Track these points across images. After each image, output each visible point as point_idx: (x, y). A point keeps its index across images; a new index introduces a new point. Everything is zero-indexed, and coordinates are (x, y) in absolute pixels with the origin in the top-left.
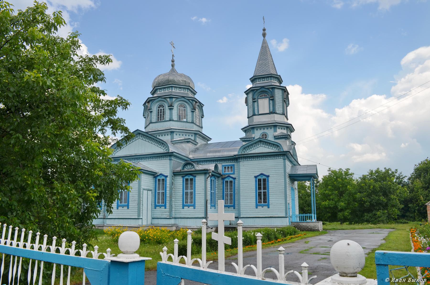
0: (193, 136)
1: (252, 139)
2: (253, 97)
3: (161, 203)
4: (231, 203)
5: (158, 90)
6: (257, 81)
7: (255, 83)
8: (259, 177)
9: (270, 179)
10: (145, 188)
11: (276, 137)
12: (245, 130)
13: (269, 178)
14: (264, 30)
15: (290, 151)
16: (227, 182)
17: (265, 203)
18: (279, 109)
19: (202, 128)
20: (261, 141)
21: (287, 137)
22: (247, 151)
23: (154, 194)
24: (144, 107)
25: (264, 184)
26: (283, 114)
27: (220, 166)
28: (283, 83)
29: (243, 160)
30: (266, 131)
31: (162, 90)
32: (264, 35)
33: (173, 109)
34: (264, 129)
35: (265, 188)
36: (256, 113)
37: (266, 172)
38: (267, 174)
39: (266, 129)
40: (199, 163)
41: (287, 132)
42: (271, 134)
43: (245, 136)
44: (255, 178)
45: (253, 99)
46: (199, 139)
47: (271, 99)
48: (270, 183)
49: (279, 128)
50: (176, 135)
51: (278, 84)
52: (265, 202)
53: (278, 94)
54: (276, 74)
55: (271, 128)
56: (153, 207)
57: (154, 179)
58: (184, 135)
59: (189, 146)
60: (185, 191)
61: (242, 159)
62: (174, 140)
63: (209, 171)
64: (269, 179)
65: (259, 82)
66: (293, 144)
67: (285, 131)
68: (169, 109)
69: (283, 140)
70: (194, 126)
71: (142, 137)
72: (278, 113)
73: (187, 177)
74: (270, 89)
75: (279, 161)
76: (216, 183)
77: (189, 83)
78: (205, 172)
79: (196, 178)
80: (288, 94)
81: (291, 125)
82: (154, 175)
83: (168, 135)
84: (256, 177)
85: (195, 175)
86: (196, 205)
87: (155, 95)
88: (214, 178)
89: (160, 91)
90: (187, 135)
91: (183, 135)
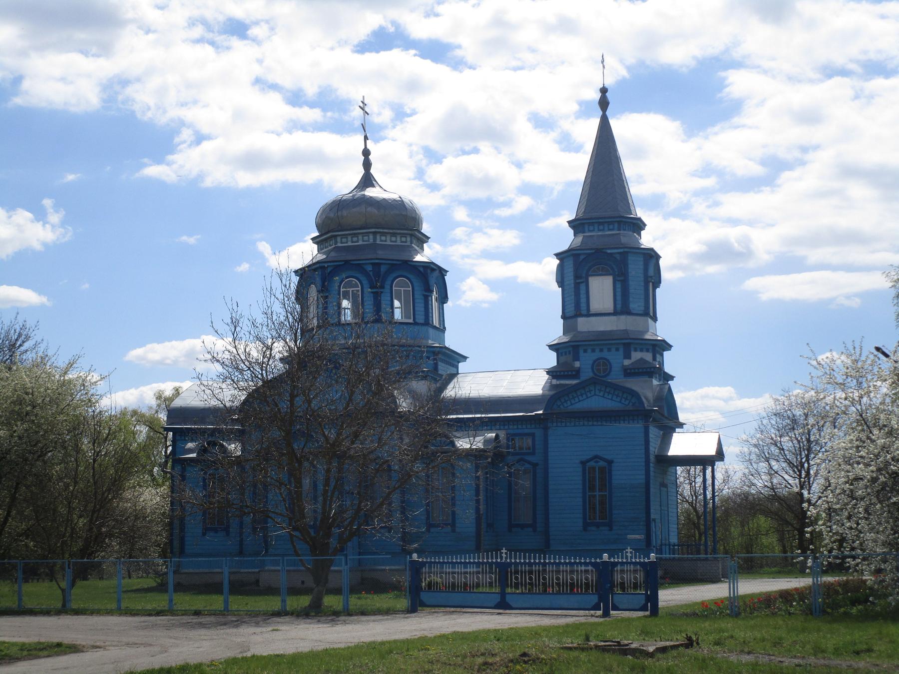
8: (592, 464)
11: (629, 371)
13: (613, 464)
31: (349, 238)
33: (382, 292)
36: (584, 311)
49: (636, 350)
55: (617, 350)
60: (588, 494)
68: (372, 292)
75: (637, 426)
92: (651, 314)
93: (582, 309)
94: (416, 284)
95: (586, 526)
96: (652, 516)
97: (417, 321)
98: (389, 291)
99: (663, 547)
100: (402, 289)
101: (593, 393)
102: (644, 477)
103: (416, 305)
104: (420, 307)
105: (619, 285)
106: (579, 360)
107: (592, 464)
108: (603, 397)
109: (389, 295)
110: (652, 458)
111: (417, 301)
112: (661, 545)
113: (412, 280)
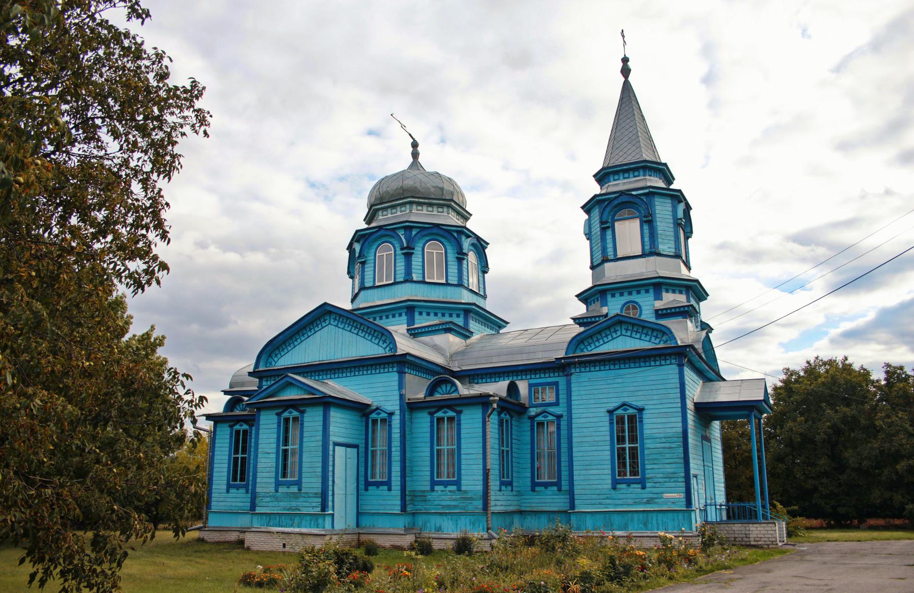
0: (462, 316)
1: (597, 319)
2: (601, 218)
3: (448, 477)
4: (382, 476)
5: (380, 213)
6: (612, 178)
7: (607, 185)
8: (620, 412)
9: (646, 415)
10: (340, 440)
11: (660, 312)
12: (584, 297)
13: (644, 412)
14: (625, 60)
15: (696, 346)
16: (375, 422)
17: (635, 475)
18: (665, 247)
19: (484, 297)
20: (621, 323)
21: (689, 312)
22: (589, 348)
23: (362, 455)
24: (350, 252)
25: (632, 427)
26: (677, 256)
27: (523, 387)
28: (675, 182)
29: (578, 370)
30: (635, 297)
32: (626, 71)
33: (413, 253)
34: (630, 293)
35: (633, 439)
37: (634, 398)
38: (640, 404)
39: (634, 293)
40: (474, 379)
41: (688, 300)
42: (648, 306)
43: (585, 311)
44: (608, 414)
45: (602, 223)
46: (477, 324)
47: (645, 222)
48: (645, 427)
49: (667, 291)
50: (421, 313)
51: (663, 185)
52: (634, 473)
53: (663, 210)
54: (654, 159)
55: (647, 291)
56: (362, 487)
57: (364, 419)
58: (440, 315)
59: (452, 341)
61: (575, 368)
62: (416, 326)
63: (492, 398)
64: (644, 416)
65: (626, 181)
66: (706, 327)
67: (680, 299)
68: (403, 254)
69: (680, 319)
70: (465, 293)
71: (335, 319)
72: (665, 253)
73: (440, 414)
74: (642, 197)
75: (668, 371)
76: (514, 428)
77: (452, 194)
78: (483, 401)
79: (463, 417)
80: (688, 208)
81: (697, 281)
82: (361, 410)
83: (400, 315)
84: (610, 412)
85: (458, 409)
86: (463, 482)
87: (373, 225)
88: (508, 417)
89: (385, 213)
90: (447, 315)
91: (436, 314)
92: (684, 258)
93: (609, 254)
94: (449, 247)
95: (615, 484)
96: (692, 472)
97: (449, 282)
98: (421, 253)
99: (709, 507)
100: (435, 251)
101: (619, 333)
102: (680, 425)
103: (449, 267)
104: (453, 269)
105: (646, 227)
106: (607, 306)
107: (620, 412)
108: (631, 337)
109: (421, 256)
110: (690, 405)
111: (449, 263)
112: (706, 505)
113: (446, 243)
